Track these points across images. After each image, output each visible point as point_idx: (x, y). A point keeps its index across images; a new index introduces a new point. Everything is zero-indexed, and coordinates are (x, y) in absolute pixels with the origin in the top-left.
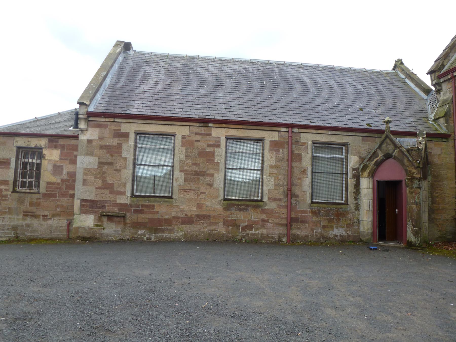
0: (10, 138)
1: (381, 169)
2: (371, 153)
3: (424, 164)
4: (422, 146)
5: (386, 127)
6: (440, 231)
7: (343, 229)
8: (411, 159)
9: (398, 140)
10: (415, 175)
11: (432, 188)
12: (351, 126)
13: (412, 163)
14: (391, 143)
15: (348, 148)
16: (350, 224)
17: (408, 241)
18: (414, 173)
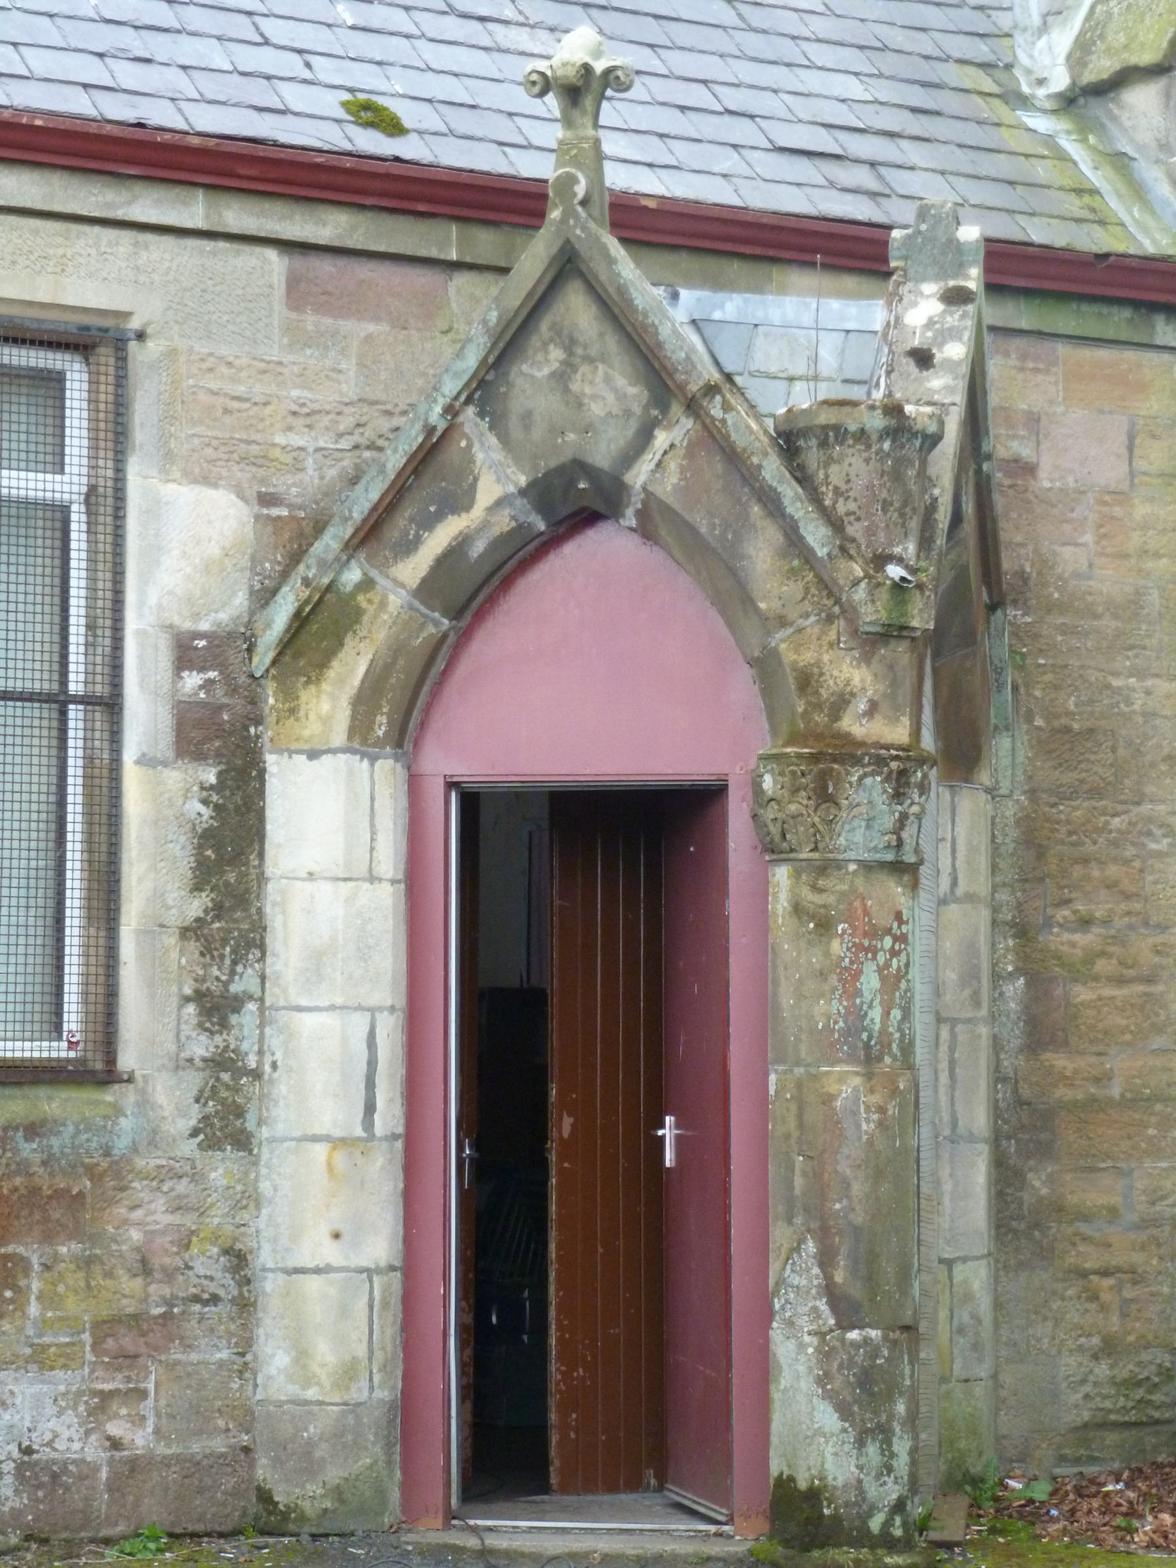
0: (403, 900)
1: (504, 636)
2: (395, 460)
3: (954, 603)
4: (938, 395)
5: (562, 151)
6: (1110, 1348)
7: (63, 1380)
8: (816, 535)
9: (688, 311)
10: (854, 725)
11: (1037, 860)
12: (160, 115)
13: (827, 587)
14: (612, 343)
15: (121, 380)
16: (136, 1320)
17: (785, 1484)
18: (842, 702)
